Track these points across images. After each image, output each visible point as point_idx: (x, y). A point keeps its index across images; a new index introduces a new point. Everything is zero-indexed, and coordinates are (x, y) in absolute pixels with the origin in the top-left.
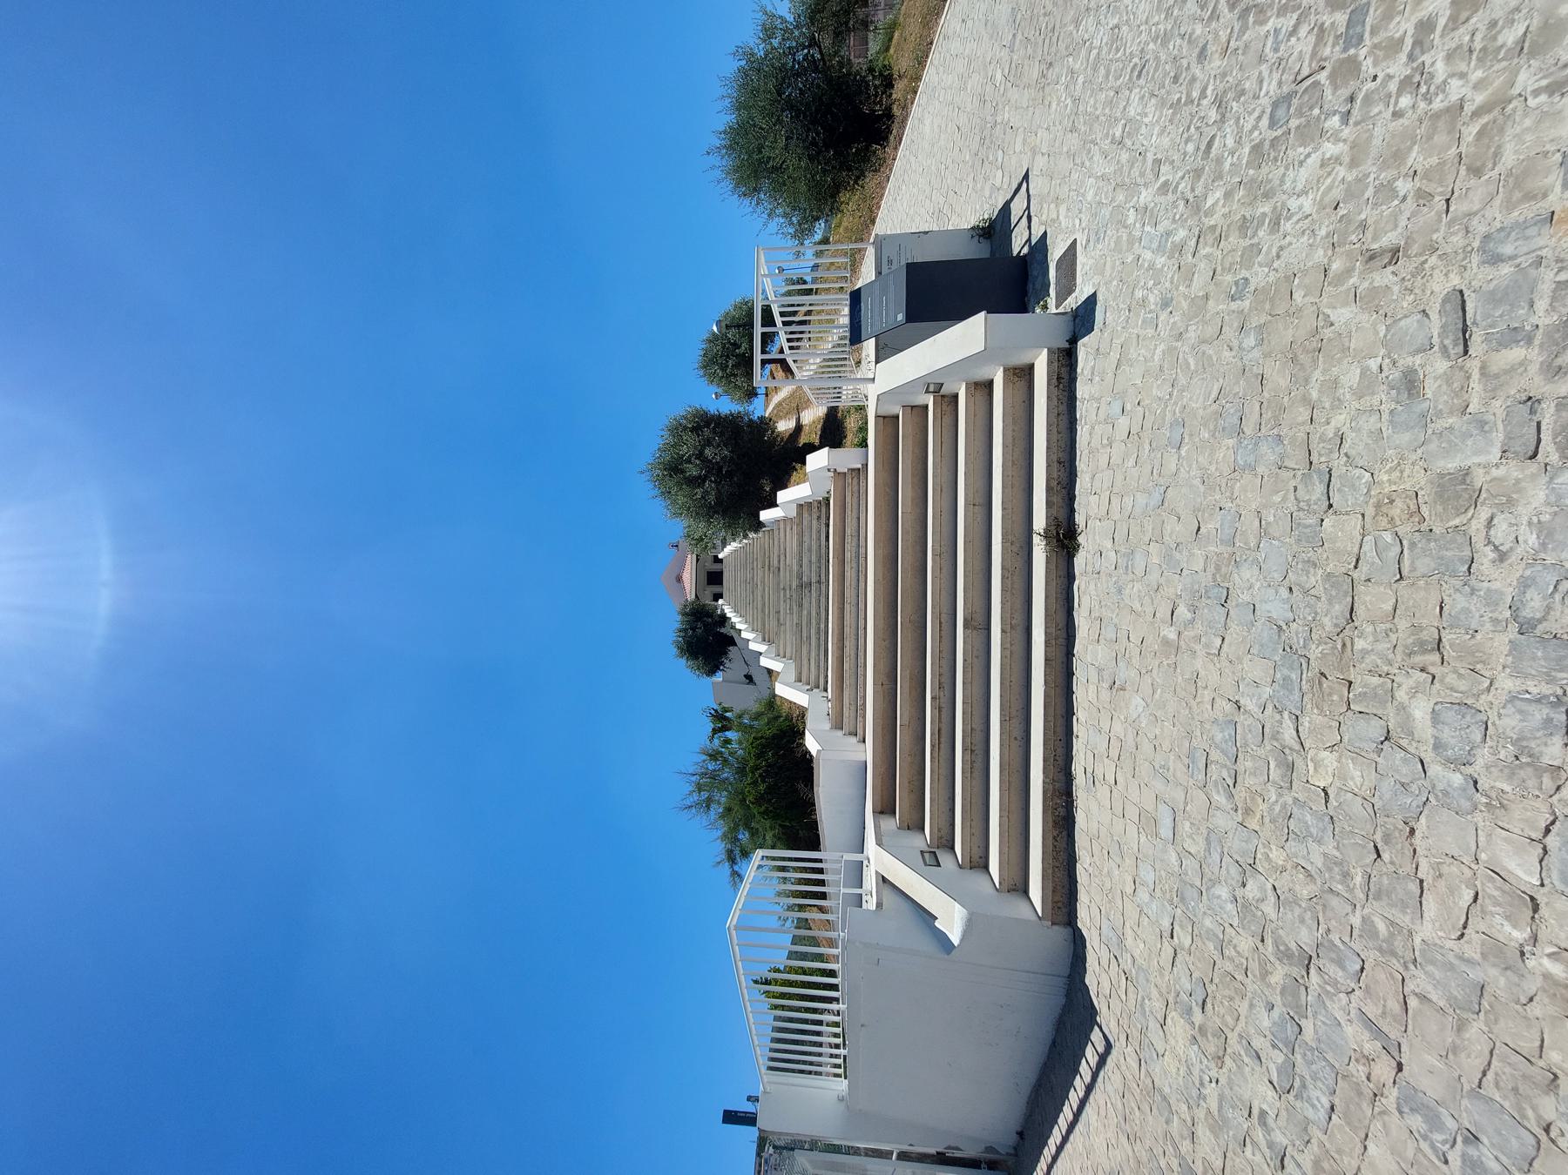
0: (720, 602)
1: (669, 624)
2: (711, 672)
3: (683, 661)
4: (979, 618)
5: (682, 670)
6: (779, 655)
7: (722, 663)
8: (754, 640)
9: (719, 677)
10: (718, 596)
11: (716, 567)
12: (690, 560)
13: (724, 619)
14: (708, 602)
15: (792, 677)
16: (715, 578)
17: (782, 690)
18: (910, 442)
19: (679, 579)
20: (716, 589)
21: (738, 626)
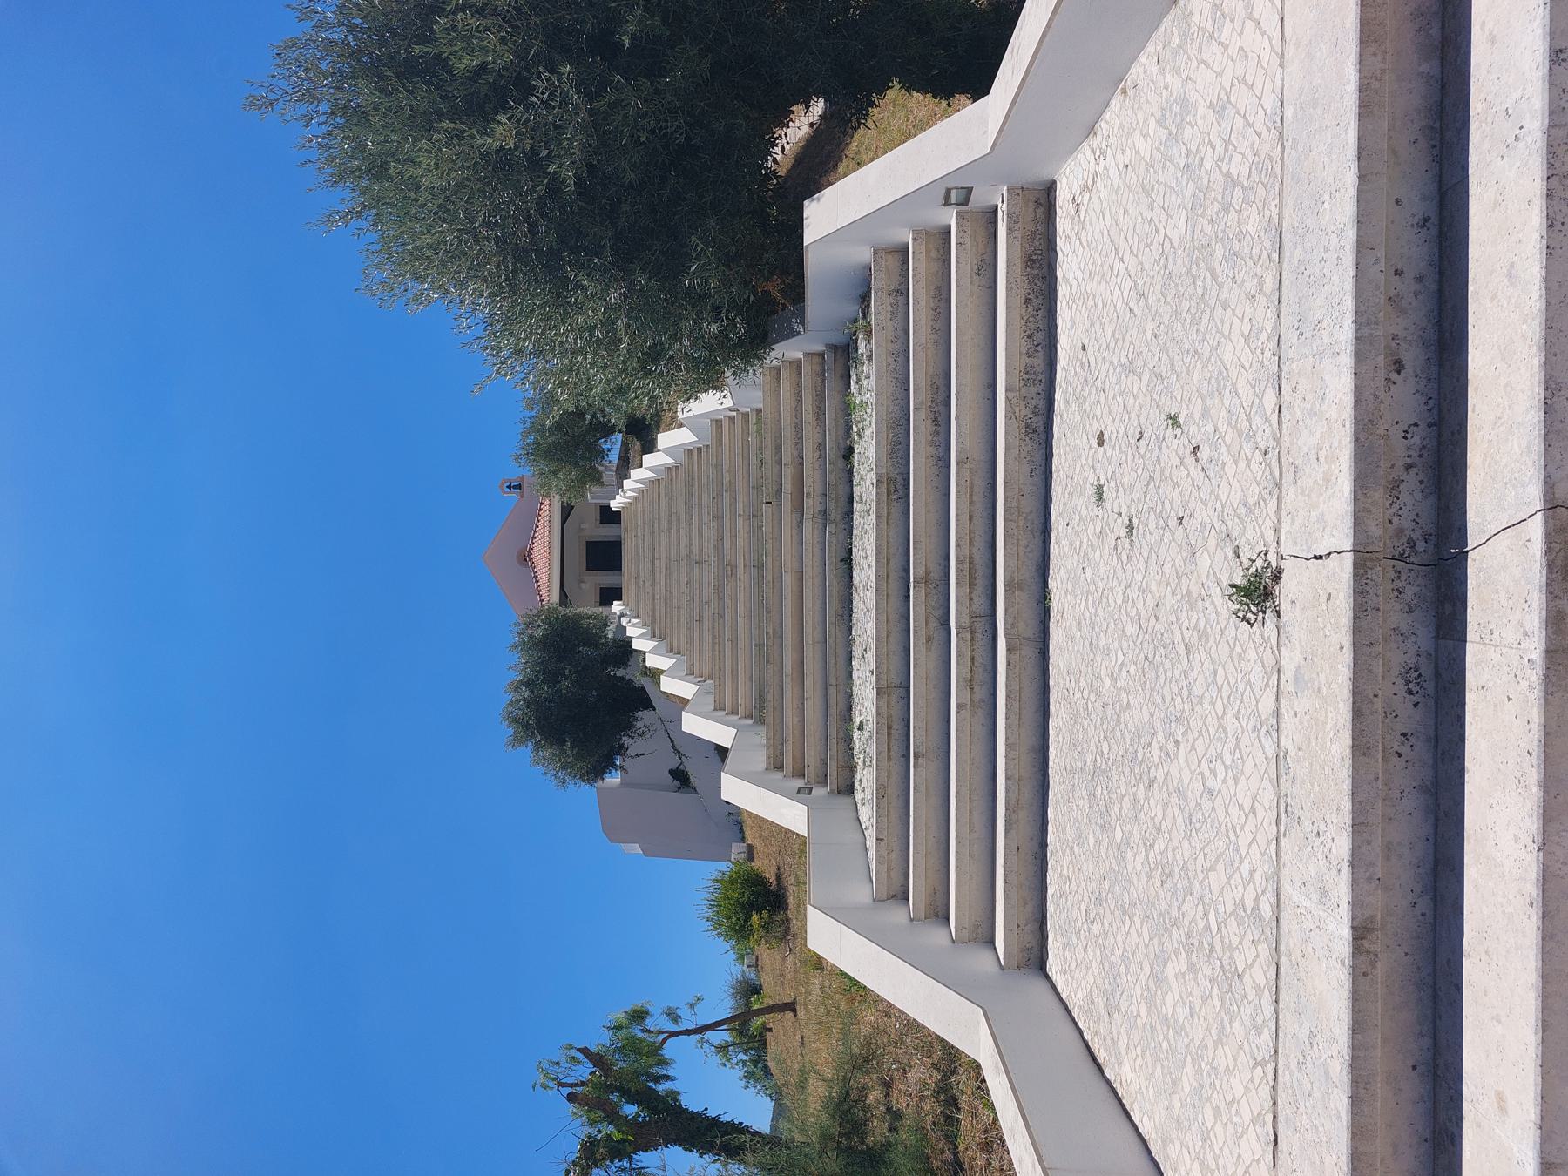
0: (617, 607)
1: (501, 670)
2: (596, 771)
3: (526, 751)
4: (936, 575)
5: (527, 770)
6: (722, 709)
7: (621, 750)
8: (671, 672)
9: (613, 779)
10: (609, 595)
11: (606, 532)
12: (550, 510)
13: (624, 651)
14: (588, 608)
15: (760, 760)
16: (604, 555)
17: (736, 790)
18: (923, 284)
19: (525, 558)
20: (606, 579)
21: (653, 661)
